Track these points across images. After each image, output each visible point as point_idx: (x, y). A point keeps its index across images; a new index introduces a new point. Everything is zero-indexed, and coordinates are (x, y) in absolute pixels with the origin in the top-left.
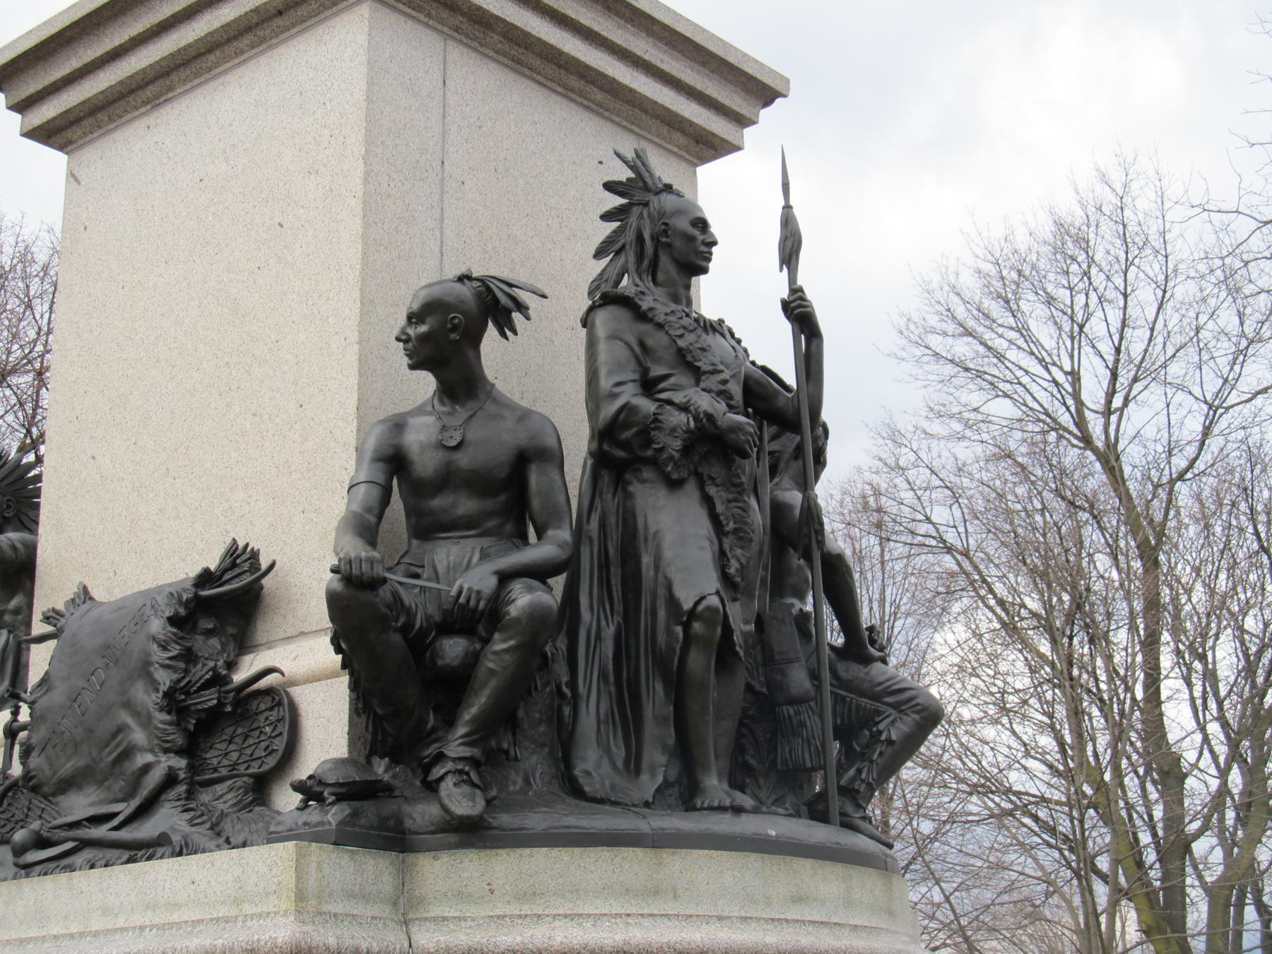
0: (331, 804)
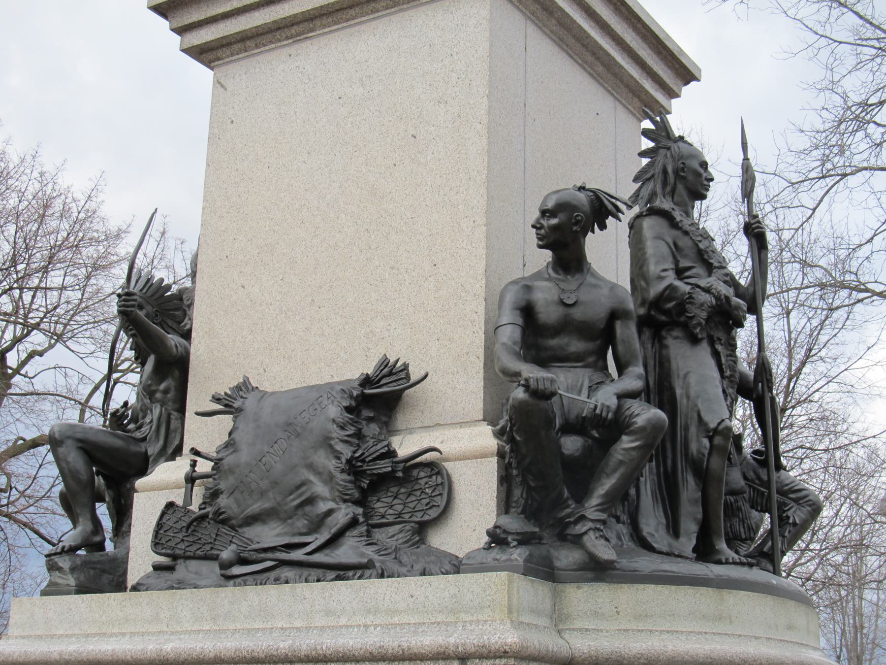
0: (514, 547)
